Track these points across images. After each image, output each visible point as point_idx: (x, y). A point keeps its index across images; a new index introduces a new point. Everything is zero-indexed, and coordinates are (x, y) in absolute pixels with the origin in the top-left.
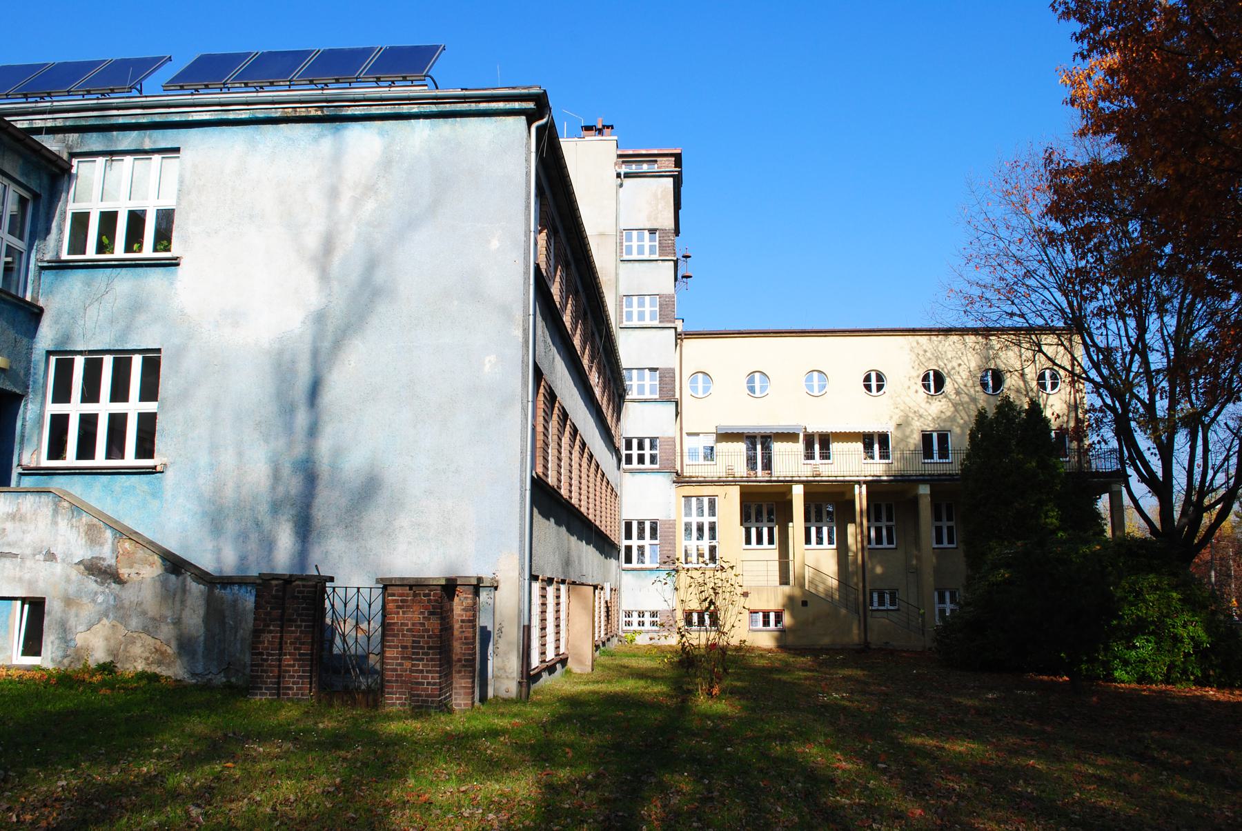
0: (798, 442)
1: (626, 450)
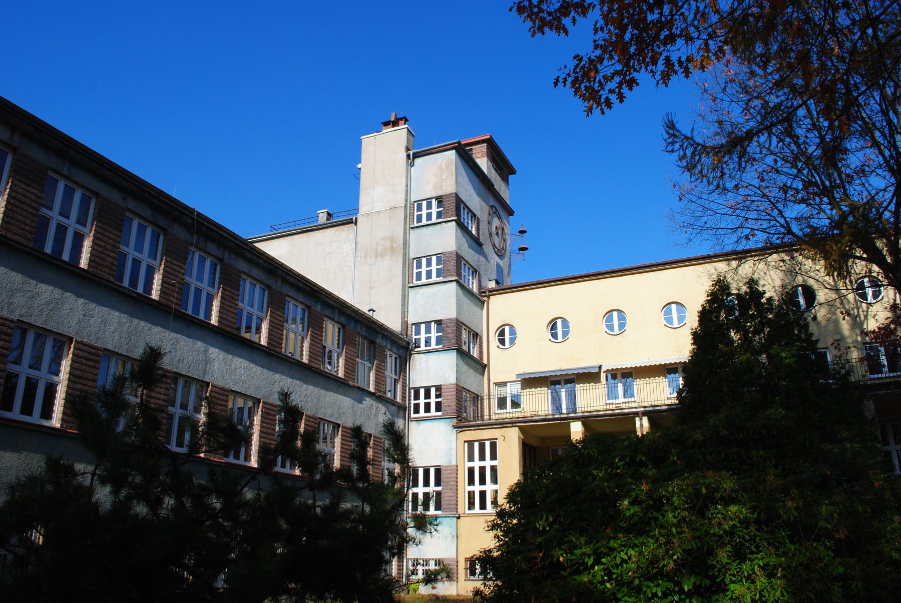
0: (599, 382)
1: (414, 400)
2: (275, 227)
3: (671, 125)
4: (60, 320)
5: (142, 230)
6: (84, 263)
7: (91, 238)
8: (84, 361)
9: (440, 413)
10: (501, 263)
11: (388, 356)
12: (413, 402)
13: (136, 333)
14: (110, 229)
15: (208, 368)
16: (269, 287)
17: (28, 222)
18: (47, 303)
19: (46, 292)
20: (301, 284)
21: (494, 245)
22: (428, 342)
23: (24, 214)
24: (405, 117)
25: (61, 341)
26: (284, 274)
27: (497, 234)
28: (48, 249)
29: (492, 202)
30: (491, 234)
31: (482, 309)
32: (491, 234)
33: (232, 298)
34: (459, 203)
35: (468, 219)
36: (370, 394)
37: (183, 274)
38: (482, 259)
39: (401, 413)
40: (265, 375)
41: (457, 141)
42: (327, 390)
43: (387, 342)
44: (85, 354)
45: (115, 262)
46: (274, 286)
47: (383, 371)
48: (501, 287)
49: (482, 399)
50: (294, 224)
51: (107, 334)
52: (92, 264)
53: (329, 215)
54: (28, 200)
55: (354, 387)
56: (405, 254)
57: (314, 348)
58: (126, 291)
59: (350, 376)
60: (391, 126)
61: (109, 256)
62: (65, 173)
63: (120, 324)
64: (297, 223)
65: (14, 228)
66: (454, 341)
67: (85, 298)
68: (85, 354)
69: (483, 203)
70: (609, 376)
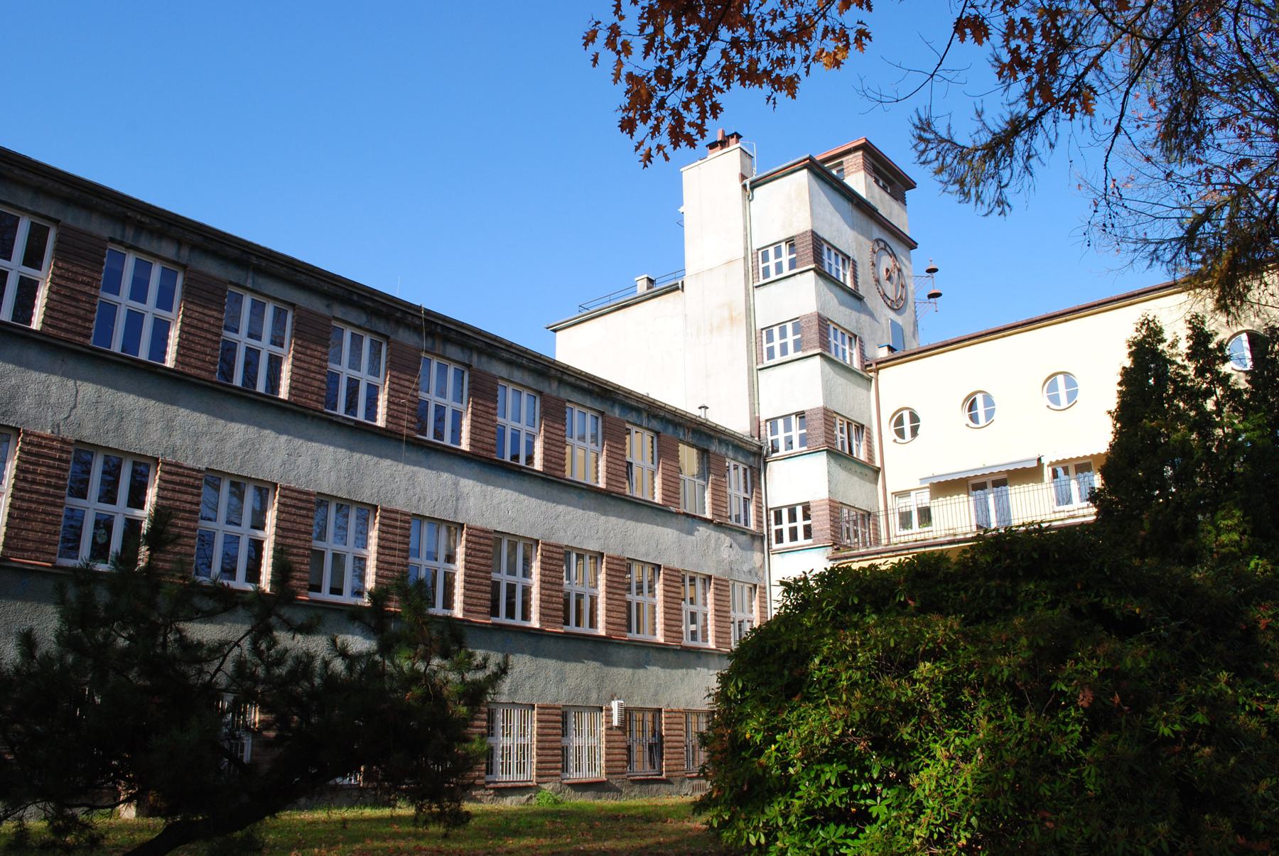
2: (585, 306)
3: (925, 126)
4: (259, 464)
5: (356, 342)
6: (284, 393)
7: (290, 360)
8: (293, 510)
9: (810, 541)
10: (899, 319)
11: (732, 468)
12: (774, 528)
13: (358, 471)
14: (313, 346)
15: (460, 505)
16: (540, 393)
17: (208, 351)
18: (241, 445)
19: (239, 432)
20: (586, 385)
21: (884, 296)
22: (789, 443)
23: (203, 342)
24: (736, 133)
25: (264, 489)
26: (559, 374)
27: (889, 278)
28: (238, 381)
29: (877, 233)
30: (877, 281)
31: (869, 390)
32: (877, 281)
33: (488, 413)
34: (818, 244)
35: (837, 263)
36: (706, 521)
37: (416, 390)
38: (864, 318)
39: (757, 544)
40: (543, 508)
41: (807, 156)
42: (637, 521)
43: (727, 449)
44: (293, 502)
45: (324, 386)
46: (547, 391)
47: (723, 489)
48: (896, 354)
49: (877, 516)
50: (608, 298)
51: (320, 475)
52: (293, 392)
53: (651, 281)
54: (206, 326)
55: (678, 513)
56: (749, 325)
57: (613, 466)
58: (340, 420)
59: (673, 500)
60: (719, 147)
61: (314, 379)
62: (249, 285)
63: (337, 462)
64: (612, 297)
65: (193, 360)
66: (822, 440)
67: (289, 434)
68: (293, 502)
69: (861, 238)
70: (1061, 472)
